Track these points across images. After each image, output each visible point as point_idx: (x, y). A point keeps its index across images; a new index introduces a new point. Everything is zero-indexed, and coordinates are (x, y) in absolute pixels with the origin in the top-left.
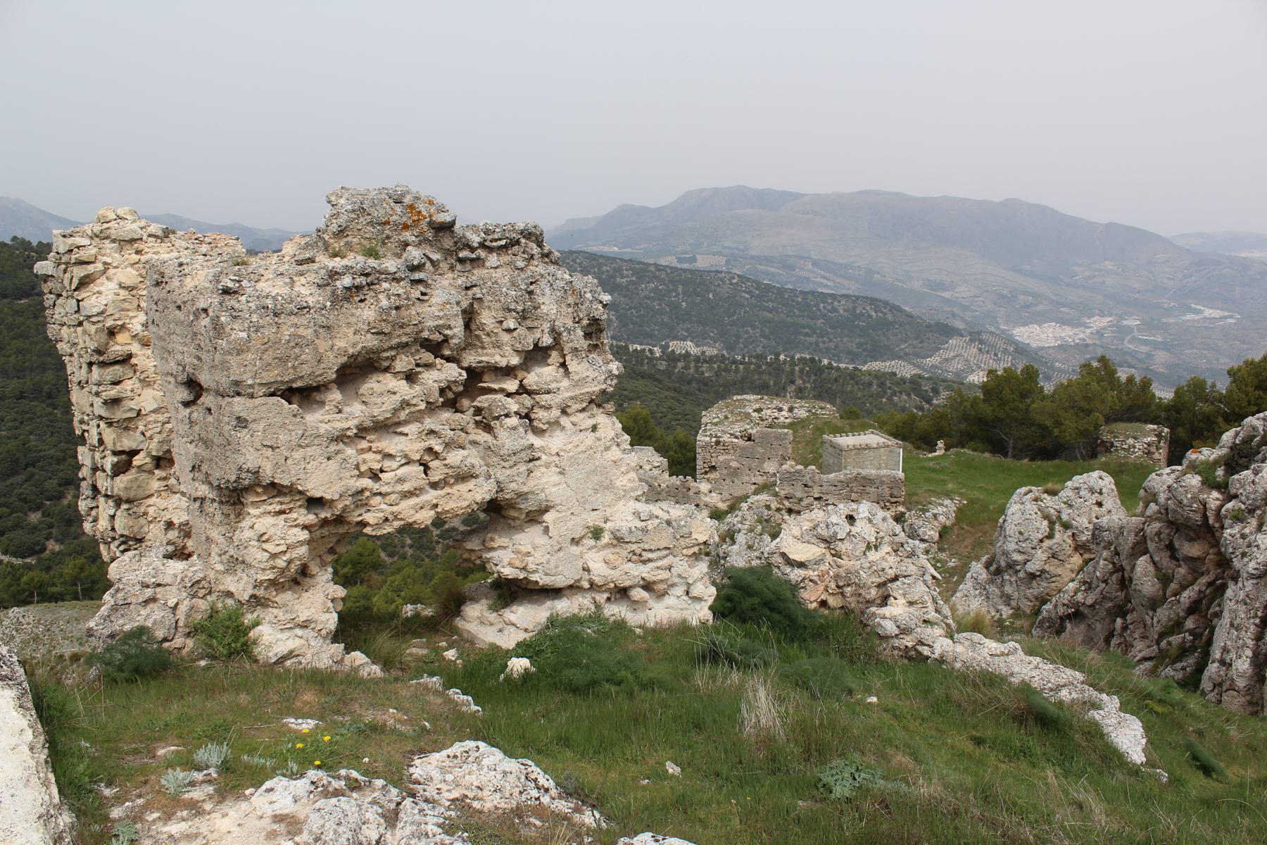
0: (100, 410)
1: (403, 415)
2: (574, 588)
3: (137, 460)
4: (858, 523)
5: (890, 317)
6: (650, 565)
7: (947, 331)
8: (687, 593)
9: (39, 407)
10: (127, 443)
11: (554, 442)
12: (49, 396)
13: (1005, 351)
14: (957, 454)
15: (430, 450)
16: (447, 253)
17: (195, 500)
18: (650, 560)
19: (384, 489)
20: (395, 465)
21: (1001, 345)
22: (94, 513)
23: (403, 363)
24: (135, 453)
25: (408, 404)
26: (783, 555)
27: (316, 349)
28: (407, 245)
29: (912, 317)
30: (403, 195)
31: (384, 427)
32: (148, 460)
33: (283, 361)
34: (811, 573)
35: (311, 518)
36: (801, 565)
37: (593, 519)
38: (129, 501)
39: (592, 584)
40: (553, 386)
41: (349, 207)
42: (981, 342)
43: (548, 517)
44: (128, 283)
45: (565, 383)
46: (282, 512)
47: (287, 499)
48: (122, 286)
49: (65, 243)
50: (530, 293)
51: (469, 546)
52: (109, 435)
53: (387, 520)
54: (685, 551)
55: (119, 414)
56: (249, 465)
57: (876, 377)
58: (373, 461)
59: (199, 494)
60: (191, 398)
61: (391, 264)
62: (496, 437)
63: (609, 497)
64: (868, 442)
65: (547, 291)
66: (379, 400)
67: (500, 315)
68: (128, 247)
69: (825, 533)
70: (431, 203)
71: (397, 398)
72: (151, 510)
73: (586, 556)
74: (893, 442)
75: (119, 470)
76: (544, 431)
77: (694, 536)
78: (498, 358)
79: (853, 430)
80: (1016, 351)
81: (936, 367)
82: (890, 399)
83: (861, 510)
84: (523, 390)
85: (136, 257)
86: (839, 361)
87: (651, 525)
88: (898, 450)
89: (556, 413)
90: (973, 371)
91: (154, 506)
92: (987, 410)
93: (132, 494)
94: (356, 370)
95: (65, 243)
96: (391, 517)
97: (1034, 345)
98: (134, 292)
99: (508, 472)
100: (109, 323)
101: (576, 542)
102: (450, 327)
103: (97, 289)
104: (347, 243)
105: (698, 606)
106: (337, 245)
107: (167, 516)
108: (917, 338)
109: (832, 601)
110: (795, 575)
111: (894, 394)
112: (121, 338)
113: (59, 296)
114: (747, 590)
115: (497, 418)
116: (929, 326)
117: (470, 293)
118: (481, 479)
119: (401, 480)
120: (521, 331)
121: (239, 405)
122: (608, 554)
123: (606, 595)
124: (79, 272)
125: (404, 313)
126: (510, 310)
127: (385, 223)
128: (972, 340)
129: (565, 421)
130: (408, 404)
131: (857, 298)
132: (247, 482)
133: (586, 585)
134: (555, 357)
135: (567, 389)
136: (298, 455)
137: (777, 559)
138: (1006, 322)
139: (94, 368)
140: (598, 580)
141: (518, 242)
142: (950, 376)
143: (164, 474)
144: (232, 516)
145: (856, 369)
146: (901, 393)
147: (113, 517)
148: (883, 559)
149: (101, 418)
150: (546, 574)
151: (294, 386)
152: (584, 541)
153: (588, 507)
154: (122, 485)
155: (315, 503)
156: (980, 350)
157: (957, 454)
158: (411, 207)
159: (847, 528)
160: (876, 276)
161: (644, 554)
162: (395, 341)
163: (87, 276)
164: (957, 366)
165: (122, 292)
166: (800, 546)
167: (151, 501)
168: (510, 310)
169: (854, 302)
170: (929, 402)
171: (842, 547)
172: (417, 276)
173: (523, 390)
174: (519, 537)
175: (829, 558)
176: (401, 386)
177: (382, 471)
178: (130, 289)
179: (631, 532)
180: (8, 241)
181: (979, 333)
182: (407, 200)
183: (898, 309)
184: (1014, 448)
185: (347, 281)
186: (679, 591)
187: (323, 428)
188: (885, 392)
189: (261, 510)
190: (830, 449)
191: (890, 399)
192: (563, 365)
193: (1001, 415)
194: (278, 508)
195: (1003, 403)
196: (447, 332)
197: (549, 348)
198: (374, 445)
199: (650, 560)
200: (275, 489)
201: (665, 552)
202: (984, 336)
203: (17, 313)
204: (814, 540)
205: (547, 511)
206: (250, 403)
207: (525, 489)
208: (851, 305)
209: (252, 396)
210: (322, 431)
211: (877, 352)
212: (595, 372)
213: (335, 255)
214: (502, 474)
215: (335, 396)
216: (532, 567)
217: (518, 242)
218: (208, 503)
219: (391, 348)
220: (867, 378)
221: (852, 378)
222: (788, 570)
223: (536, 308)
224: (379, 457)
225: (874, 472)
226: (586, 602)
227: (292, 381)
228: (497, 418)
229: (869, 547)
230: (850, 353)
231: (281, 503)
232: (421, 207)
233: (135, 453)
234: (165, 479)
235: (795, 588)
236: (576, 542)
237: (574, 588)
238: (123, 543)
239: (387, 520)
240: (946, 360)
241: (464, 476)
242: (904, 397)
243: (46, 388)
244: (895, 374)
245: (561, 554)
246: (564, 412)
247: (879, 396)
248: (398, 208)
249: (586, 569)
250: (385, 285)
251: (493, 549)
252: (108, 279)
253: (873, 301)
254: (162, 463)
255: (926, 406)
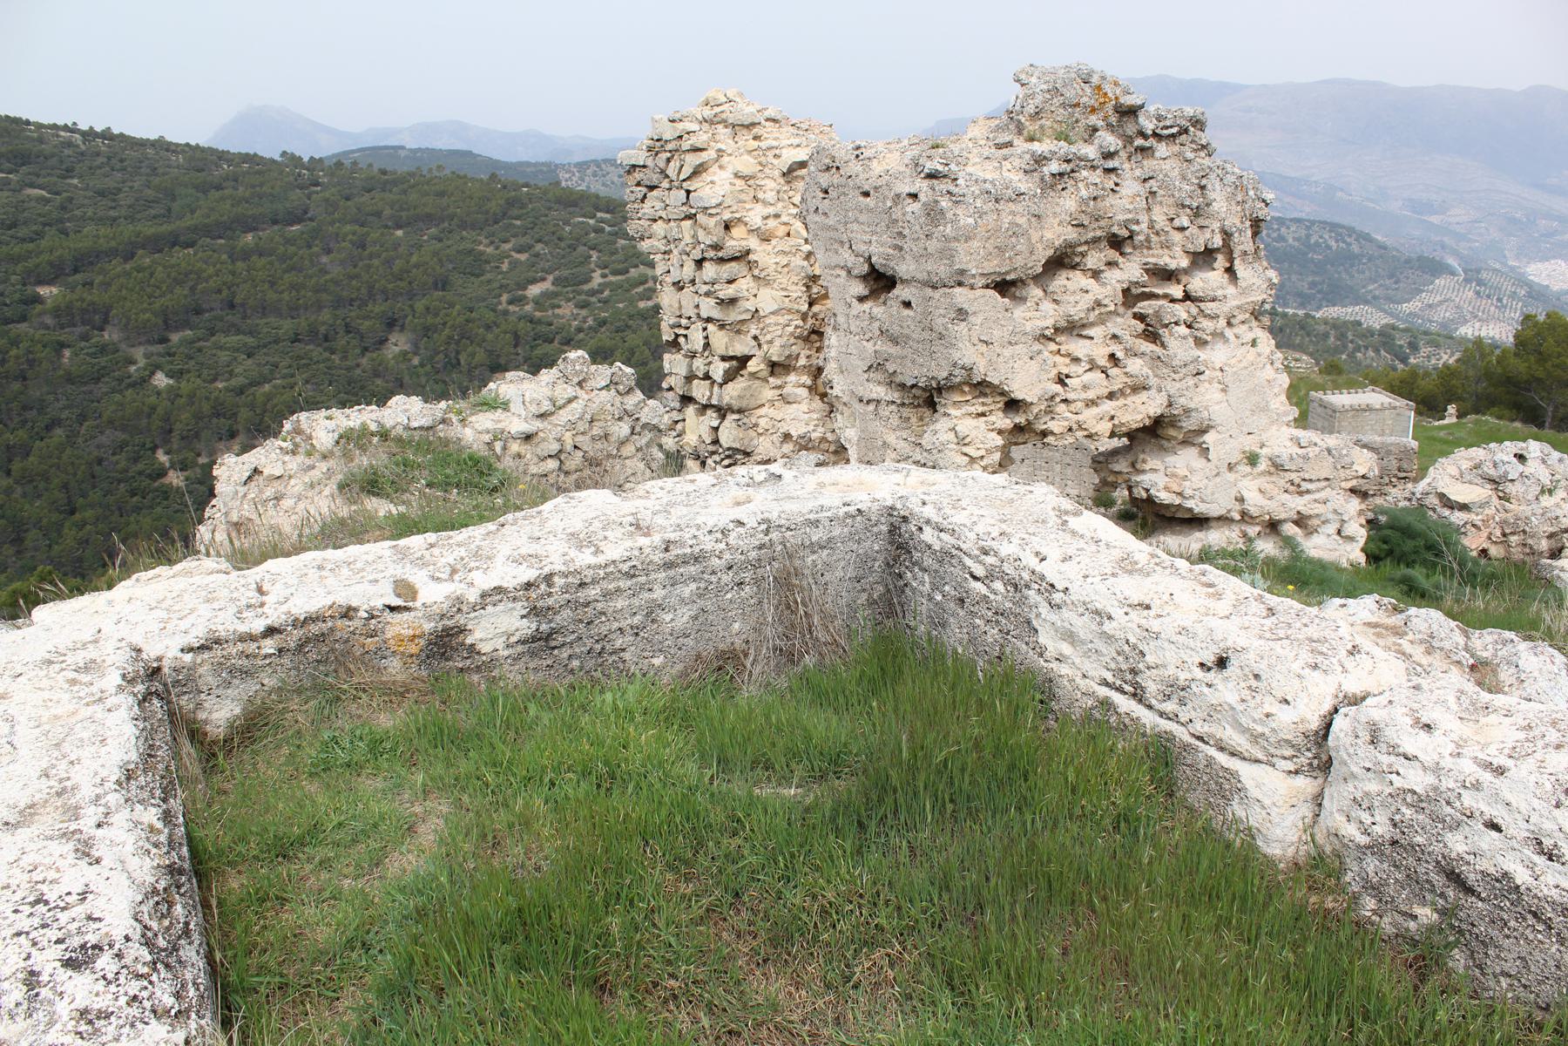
0: (708, 308)
1: (1092, 317)
2: (1224, 520)
3: (752, 366)
4: (1529, 463)
5: (1355, 248)
6: (1307, 497)
7: (1435, 268)
8: (1339, 532)
9: (316, 351)
10: (739, 349)
11: (1216, 355)
12: (326, 339)
13: (1513, 295)
14: (1476, 422)
15: (1112, 356)
16: (1129, 140)
17: (868, 402)
18: (1308, 492)
19: (1071, 396)
20: (1080, 370)
21: (1508, 287)
22: (679, 426)
23: (1094, 260)
24: (748, 358)
25: (1099, 305)
26: (1442, 496)
27: (1029, 239)
28: (1095, 130)
29: (1385, 248)
30: (1089, 75)
31: (1073, 328)
32: (762, 366)
33: (1001, 250)
34: (1473, 516)
35: (1006, 422)
36: (1464, 507)
37: (1250, 444)
38: (740, 411)
39: (1244, 514)
40: (1219, 293)
41: (1045, 87)
42: (1480, 283)
43: (1209, 438)
44: (746, 171)
45: (1231, 290)
46: (983, 414)
47: (989, 400)
48: (737, 175)
49: (675, 129)
50: (1203, 188)
51: (1117, 468)
52: (720, 340)
53: (1070, 430)
54: (1343, 484)
55: (733, 316)
56: (967, 361)
57: (1334, 326)
58: (1064, 366)
59: (874, 396)
60: (866, 292)
61: (1090, 151)
62: (1163, 346)
63: (1264, 420)
64: (1370, 402)
65: (1218, 187)
66: (1072, 299)
67: (1172, 212)
68: (745, 131)
69: (1492, 472)
70: (1116, 84)
71: (1090, 298)
72: (763, 422)
73: (1240, 484)
74: (1401, 402)
75: (729, 377)
76: (1206, 342)
77: (1355, 467)
78: (1167, 260)
79: (1337, 387)
80: (1529, 295)
81: (1415, 315)
82: (1351, 356)
83: (1531, 449)
84: (1187, 297)
85: (756, 144)
86: (1285, 305)
87: (1312, 452)
88: (1406, 410)
89: (1222, 322)
90: (1466, 321)
91: (764, 417)
92: (1520, 367)
93: (744, 404)
94: (1061, 261)
95: (675, 129)
96: (1075, 427)
97: (1555, 288)
98: (751, 182)
99: (1178, 385)
100: (727, 216)
101: (1230, 467)
102: (1138, 223)
103: (709, 179)
104: (1042, 127)
105: (1348, 547)
106: (1031, 127)
107: (784, 428)
108: (1391, 276)
109: (1494, 551)
110: (1458, 517)
111: (1358, 349)
112: (737, 232)
113: (652, 188)
114: (1407, 532)
115: (1166, 326)
116: (1408, 261)
117: (1147, 185)
118: (1153, 392)
119: (1085, 387)
120: (1193, 230)
121: (961, 296)
122: (1262, 482)
123: (1258, 529)
124: (692, 160)
125: (1100, 204)
126: (1183, 206)
127: (1078, 105)
128: (1467, 281)
129: (1229, 333)
130: (1099, 305)
131: (1313, 223)
132: (958, 380)
133: (1238, 517)
134: (1221, 261)
135: (1235, 298)
136: (1007, 352)
137: (1433, 501)
138: (1517, 257)
139: (707, 265)
140: (1254, 511)
141: (1186, 131)
142: (1433, 328)
143: (779, 382)
144: (914, 420)
145: (1307, 315)
146: (1366, 348)
147: (716, 429)
148: (1557, 505)
149: (709, 320)
150: (1203, 501)
151: (1008, 278)
152: (1239, 468)
153: (1246, 430)
154: (735, 394)
155: (1012, 405)
156: (1478, 293)
157: (1476, 422)
158: (1099, 88)
159: (1521, 468)
160: (1339, 194)
161: (927, 529)
162: (1091, 235)
163: (701, 165)
164: (1444, 314)
165: (740, 183)
166: (1460, 486)
167: (762, 411)
168: (1183, 206)
169: (1308, 228)
170: (1404, 360)
171: (1511, 489)
172: (1110, 164)
173: (1187, 297)
174: (1171, 460)
175: (1495, 500)
176: (1089, 283)
177: (1067, 376)
178: (746, 178)
179: (1292, 459)
180: (277, 158)
181: (1478, 271)
182: (1095, 80)
183: (1368, 238)
184: (1554, 417)
185: (1054, 167)
186: (1331, 529)
187: (1028, 327)
188: (1345, 347)
189: (964, 411)
190: (1320, 410)
191: (1351, 356)
192: (1230, 271)
193: (1540, 374)
194: (981, 409)
195: (1542, 357)
196: (1134, 227)
197: (1217, 250)
198: (1063, 349)
199: (1308, 492)
200: (982, 388)
201: (1324, 484)
202: (1484, 275)
203: (289, 241)
204: (1480, 481)
205: (1204, 432)
206: (971, 294)
207: (1192, 406)
208: (1303, 232)
209: (972, 288)
210: (1028, 329)
211: (1336, 295)
212: (1257, 280)
213: (1031, 139)
214: (1172, 388)
215: (1035, 292)
216: (1188, 492)
217: (1186, 131)
218: (883, 405)
219: (1086, 242)
220: (1322, 328)
221: (1302, 328)
222: (1446, 512)
223: (1208, 205)
224: (1067, 360)
225: (1378, 439)
226: (1234, 535)
227: (1007, 273)
228: (1166, 326)
229: (1543, 492)
230: (1300, 295)
231: (983, 404)
232: (1108, 88)
233: (748, 358)
234: (779, 387)
235: (1459, 530)
236: (1230, 467)
237: (1224, 520)
238: (728, 457)
239: (1070, 430)
240: (1430, 306)
241: (1139, 388)
242: (1371, 353)
243: (323, 329)
244: (1359, 324)
245: (1218, 479)
246: (1229, 324)
247: (1337, 351)
248: (1087, 88)
249: (1241, 500)
250: (1085, 173)
251: (1143, 471)
252: (721, 167)
253: (1333, 227)
254: (777, 370)
255: (1401, 366)
